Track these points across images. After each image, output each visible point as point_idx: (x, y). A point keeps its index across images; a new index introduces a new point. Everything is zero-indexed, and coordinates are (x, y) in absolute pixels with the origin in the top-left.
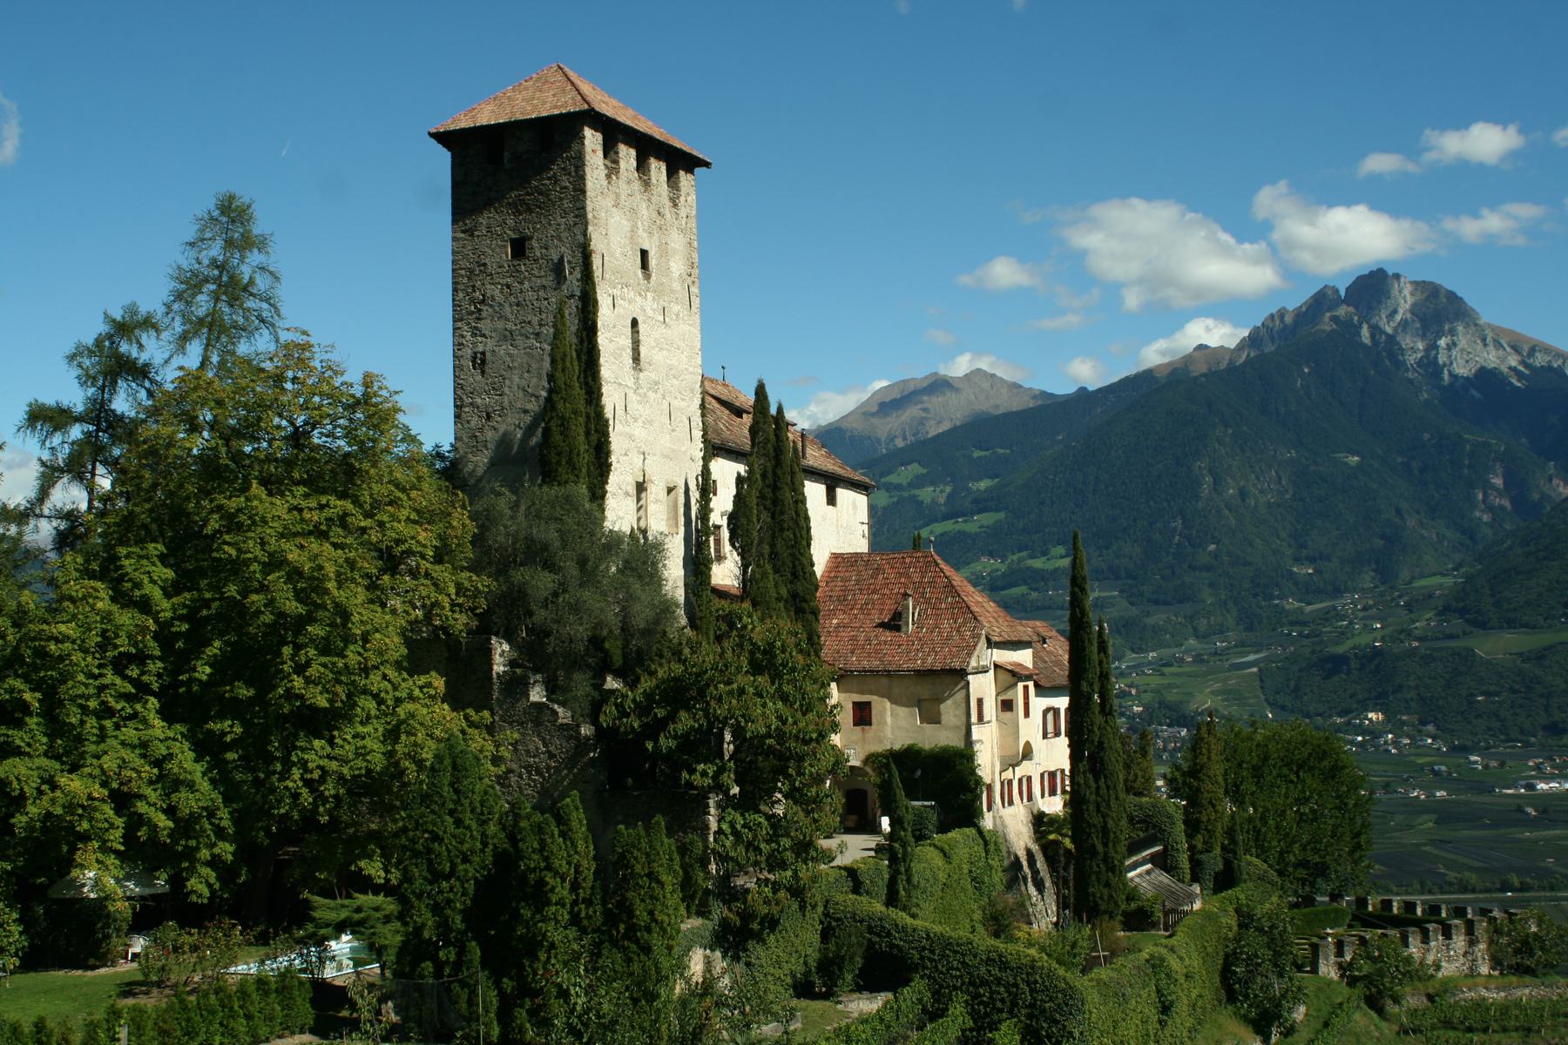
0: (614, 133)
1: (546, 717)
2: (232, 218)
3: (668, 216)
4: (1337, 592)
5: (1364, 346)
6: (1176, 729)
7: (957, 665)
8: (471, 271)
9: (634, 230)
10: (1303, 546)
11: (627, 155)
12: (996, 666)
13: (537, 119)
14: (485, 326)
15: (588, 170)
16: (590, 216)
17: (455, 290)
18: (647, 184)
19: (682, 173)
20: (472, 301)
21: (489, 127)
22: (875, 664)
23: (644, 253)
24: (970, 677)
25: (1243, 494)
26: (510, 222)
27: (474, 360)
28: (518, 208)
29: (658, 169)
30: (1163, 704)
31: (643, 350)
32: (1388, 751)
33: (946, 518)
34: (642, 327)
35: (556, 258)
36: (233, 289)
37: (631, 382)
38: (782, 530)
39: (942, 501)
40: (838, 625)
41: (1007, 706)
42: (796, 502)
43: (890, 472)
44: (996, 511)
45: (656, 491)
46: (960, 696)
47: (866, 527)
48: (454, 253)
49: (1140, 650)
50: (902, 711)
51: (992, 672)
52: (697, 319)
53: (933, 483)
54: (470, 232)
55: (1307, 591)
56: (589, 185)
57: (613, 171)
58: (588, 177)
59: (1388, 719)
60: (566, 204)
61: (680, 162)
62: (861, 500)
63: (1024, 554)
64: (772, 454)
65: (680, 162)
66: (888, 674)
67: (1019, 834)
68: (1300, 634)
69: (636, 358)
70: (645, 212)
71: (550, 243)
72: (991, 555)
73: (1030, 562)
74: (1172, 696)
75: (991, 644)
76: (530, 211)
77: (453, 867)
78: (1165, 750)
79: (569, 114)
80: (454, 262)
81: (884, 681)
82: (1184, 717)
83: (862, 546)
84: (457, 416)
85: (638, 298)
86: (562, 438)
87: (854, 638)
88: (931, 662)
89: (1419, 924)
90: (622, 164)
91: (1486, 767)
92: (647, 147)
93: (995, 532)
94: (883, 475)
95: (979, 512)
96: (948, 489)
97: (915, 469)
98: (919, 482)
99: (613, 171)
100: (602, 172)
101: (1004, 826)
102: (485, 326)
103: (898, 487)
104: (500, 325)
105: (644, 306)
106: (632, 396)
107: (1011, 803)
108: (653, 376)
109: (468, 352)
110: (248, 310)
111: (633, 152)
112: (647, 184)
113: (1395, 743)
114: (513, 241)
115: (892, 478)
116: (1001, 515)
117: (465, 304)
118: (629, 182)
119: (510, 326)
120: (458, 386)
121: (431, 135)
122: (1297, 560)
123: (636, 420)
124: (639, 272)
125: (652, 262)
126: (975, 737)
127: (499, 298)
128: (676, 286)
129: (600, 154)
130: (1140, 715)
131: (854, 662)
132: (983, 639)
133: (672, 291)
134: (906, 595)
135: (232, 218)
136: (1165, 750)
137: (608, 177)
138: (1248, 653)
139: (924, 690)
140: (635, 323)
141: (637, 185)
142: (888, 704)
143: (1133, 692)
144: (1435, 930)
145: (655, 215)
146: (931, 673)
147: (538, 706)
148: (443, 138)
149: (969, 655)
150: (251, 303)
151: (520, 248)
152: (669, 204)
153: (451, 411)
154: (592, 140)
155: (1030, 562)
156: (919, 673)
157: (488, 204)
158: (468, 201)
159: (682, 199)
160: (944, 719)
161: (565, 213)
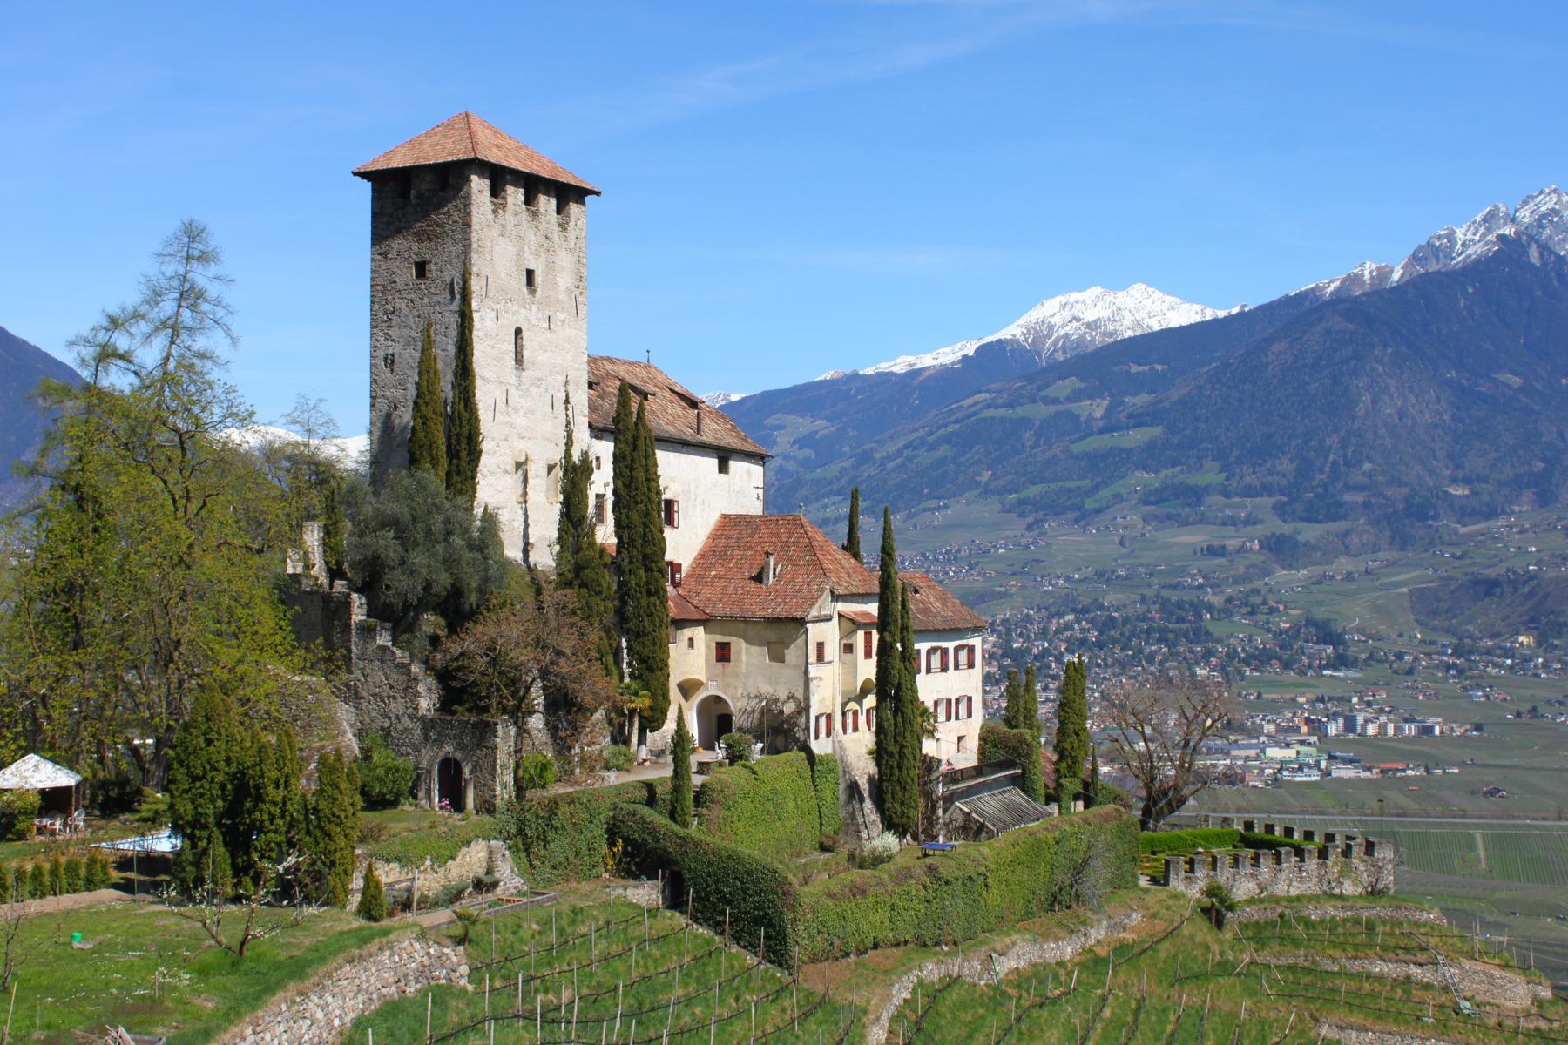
0: (499, 177)
1: (388, 656)
2: (193, 244)
3: (556, 239)
4: (1492, 513)
5: (1533, 265)
6: (1322, 646)
7: (798, 614)
8: (384, 287)
9: (520, 254)
10: (1459, 467)
11: (515, 195)
12: (840, 615)
13: (436, 165)
14: (394, 332)
15: (474, 209)
16: (474, 246)
17: (373, 302)
20: (385, 313)
21: (404, 169)
22: (736, 611)
23: (530, 274)
25: (1402, 415)
26: (415, 248)
27: (386, 359)
28: (423, 236)
29: (547, 204)
30: (1310, 622)
31: (526, 353)
32: (1536, 675)
33: (1101, 431)
34: (525, 334)
35: (448, 279)
36: (190, 295)
37: (512, 380)
38: (636, 503)
39: (1098, 414)
41: (849, 648)
42: (648, 480)
43: (1047, 386)
45: (537, 470)
46: (800, 641)
47: (761, 492)
48: (373, 271)
49: (1290, 567)
50: (755, 649)
51: (836, 619)
52: (584, 324)
53: (1091, 397)
54: (384, 254)
55: (1465, 513)
56: (475, 220)
58: (474, 213)
59: (1539, 643)
60: (457, 236)
61: (568, 194)
62: (757, 471)
63: (1178, 469)
64: (631, 439)
65: (568, 194)
66: (745, 620)
68: (1453, 556)
69: (519, 359)
70: (532, 238)
71: (443, 270)
72: (1146, 469)
74: (1320, 614)
75: (836, 598)
76: (430, 239)
77: (205, 772)
78: (1310, 667)
80: (372, 279)
81: (741, 625)
82: (1330, 634)
83: (756, 508)
84: (372, 405)
86: (434, 432)
87: (725, 588)
88: (781, 611)
89: (1272, 845)
90: (510, 200)
92: (533, 185)
93: (1151, 447)
94: (1040, 389)
95: (1135, 426)
96: (1105, 403)
97: (1072, 383)
98: (1076, 396)
100: (489, 208)
101: (842, 749)
102: (394, 332)
103: (1055, 401)
104: (406, 332)
105: (529, 316)
106: (513, 391)
107: (856, 729)
108: (537, 374)
109: (381, 354)
110: (203, 313)
113: (1545, 666)
115: (1050, 392)
116: (1157, 431)
117: (380, 314)
118: (516, 214)
119: (413, 334)
120: (373, 382)
121: (355, 174)
122: (1454, 481)
123: (516, 411)
124: (525, 289)
125: (538, 279)
126: (811, 674)
127: (405, 310)
128: (563, 297)
129: (487, 193)
130: (1287, 631)
131: (721, 609)
132: (827, 592)
134: (768, 554)
135: (193, 244)
136: (1310, 667)
137: (495, 212)
139: (772, 633)
140: (518, 331)
141: (524, 216)
142: (744, 645)
143: (1281, 608)
144: (1288, 853)
146: (778, 620)
147: (383, 648)
148: (364, 175)
149: (811, 606)
150: (205, 307)
151: (421, 269)
152: (556, 228)
153: (368, 401)
154: (479, 185)
156: (770, 621)
157: (399, 231)
158: (385, 226)
159: (572, 224)
160: (787, 658)
161: (455, 243)
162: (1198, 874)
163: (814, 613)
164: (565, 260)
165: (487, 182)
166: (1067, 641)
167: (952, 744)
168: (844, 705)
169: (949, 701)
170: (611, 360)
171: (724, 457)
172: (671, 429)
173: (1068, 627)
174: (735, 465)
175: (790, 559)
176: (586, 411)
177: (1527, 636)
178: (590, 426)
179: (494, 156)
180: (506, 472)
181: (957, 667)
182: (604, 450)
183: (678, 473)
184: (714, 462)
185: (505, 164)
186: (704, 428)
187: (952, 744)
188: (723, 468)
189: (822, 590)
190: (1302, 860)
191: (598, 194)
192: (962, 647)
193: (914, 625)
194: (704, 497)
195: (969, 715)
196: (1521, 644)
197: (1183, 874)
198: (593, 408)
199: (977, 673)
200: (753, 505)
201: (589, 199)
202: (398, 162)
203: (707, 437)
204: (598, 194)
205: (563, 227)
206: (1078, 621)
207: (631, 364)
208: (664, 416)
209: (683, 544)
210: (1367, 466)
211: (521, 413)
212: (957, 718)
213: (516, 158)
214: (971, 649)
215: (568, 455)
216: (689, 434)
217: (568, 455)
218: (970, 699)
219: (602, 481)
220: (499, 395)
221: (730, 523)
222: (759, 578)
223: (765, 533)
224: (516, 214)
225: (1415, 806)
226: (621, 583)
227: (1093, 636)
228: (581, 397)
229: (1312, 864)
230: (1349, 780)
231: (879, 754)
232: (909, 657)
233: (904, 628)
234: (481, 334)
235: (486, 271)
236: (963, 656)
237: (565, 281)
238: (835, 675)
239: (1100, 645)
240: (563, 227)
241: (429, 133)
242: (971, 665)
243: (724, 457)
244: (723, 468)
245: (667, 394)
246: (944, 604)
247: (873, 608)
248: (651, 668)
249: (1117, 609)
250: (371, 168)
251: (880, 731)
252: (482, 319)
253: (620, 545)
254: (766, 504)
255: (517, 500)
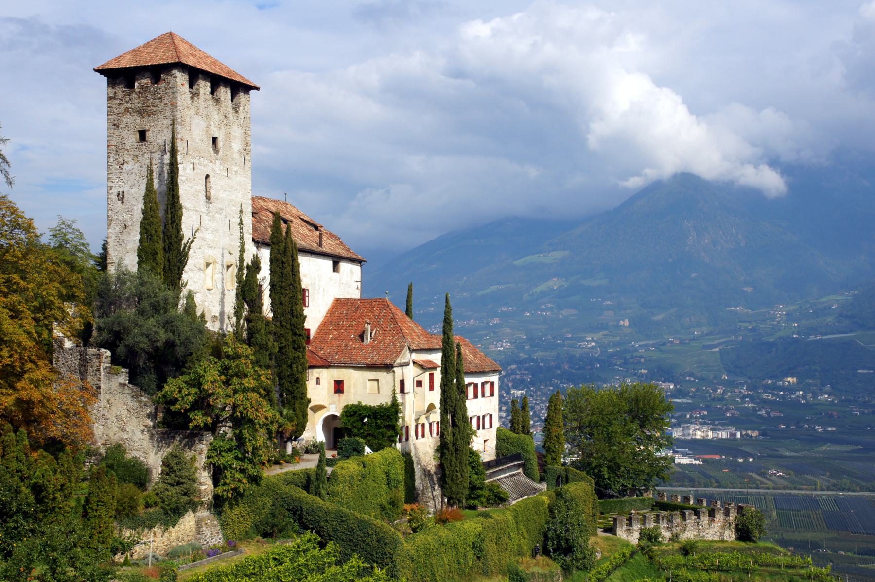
0: (194, 74)
6: (667, 384)
7: (388, 362)
9: (208, 127)
11: (204, 87)
13: (152, 66)
16: (179, 120)
18: (218, 101)
19: (241, 94)
23: (215, 140)
24: (395, 369)
27: (118, 195)
29: (225, 93)
34: (211, 179)
37: (204, 210)
40: (332, 339)
44: (564, 250)
47: (359, 284)
52: (249, 174)
57: (194, 95)
60: (168, 113)
61: (239, 88)
62: (357, 269)
67: (425, 454)
69: (208, 198)
70: (216, 116)
73: (583, 282)
75: (412, 351)
79: (168, 64)
85: (210, 164)
86: (164, 240)
87: (339, 346)
90: (202, 91)
91: (863, 413)
92: (217, 81)
95: (553, 250)
99: (194, 95)
100: (188, 95)
105: (215, 168)
106: (204, 217)
107: (423, 436)
108: (219, 206)
111: (209, 84)
112: (218, 101)
113: (804, 397)
114: (139, 132)
116: (566, 253)
118: (206, 100)
121: (96, 71)
124: (211, 150)
125: (220, 143)
128: (236, 156)
129: (187, 86)
133: (233, 159)
137: (192, 98)
138: (715, 339)
140: (207, 177)
141: (211, 102)
145: (222, 118)
148: (102, 72)
151: (142, 135)
152: (232, 111)
155: (583, 282)
159: (241, 108)
161: (166, 118)
162: (635, 527)
163: (398, 361)
164: (237, 132)
165: (187, 77)
166: (513, 381)
167: (484, 444)
168: (417, 420)
169: (479, 418)
170: (264, 200)
171: (337, 260)
172: (303, 243)
173: (513, 372)
174: (344, 266)
175: (380, 326)
176: (251, 231)
177: (793, 377)
178: (253, 240)
179: (191, 61)
180: (200, 269)
181: (483, 396)
182: (265, 255)
183: (312, 272)
184: (329, 263)
185: (199, 67)
186: (324, 243)
187: (484, 444)
188: (336, 268)
189: (403, 347)
190: (699, 518)
191: (258, 89)
192: (487, 382)
193: (465, 367)
194: (325, 286)
195: (491, 426)
196: (789, 382)
197: (625, 527)
198: (255, 229)
199: (496, 399)
200: (354, 293)
201: (252, 92)
202: (125, 63)
203: (326, 249)
204: (258, 89)
205: (236, 109)
206: (519, 369)
207: (275, 201)
208: (301, 235)
209: (314, 316)
210: (694, 275)
211: (210, 231)
212: (484, 428)
213: (205, 64)
214: (492, 384)
215: (241, 260)
216: (315, 247)
217: (241, 260)
218: (491, 416)
219: (264, 275)
220: (195, 218)
221: (339, 304)
222: (362, 337)
223: (363, 310)
224: (206, 100)
225: (790, 485)
226: (278, 342)
227: (528, 378)
228: (248, 221)
229: (705, 519)
230: (687, 465)
231: (442, 449)
232: (462, 390)
233: (459, 371)
234: (183, 178)
235: (187, 137)
236: (487, 387)
237: (237, 145)
238: (421, 403)
239: (532, 383)
240: (236, 109)
241: (147, 45)
242: (492, 395)
243: (337, 260)
244: (336, 268)
245: (299, 221)
246: (475, 356)
247: (437, 358)
248: (294, 398)
249: (543, 361)
250: (116, 66)
251: (442, 436)
252: (184, 169)
253: (274, 317)
254: (363, 290)
255: (209, 289)
